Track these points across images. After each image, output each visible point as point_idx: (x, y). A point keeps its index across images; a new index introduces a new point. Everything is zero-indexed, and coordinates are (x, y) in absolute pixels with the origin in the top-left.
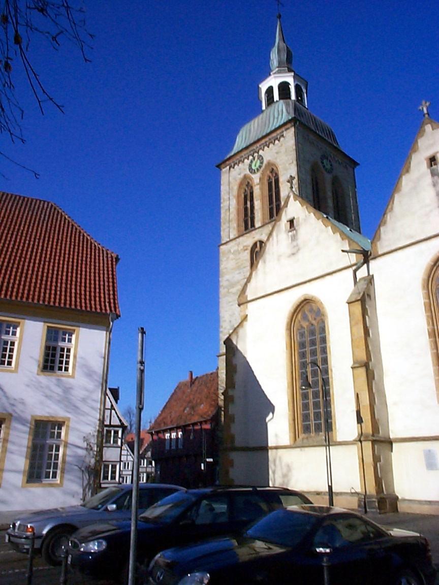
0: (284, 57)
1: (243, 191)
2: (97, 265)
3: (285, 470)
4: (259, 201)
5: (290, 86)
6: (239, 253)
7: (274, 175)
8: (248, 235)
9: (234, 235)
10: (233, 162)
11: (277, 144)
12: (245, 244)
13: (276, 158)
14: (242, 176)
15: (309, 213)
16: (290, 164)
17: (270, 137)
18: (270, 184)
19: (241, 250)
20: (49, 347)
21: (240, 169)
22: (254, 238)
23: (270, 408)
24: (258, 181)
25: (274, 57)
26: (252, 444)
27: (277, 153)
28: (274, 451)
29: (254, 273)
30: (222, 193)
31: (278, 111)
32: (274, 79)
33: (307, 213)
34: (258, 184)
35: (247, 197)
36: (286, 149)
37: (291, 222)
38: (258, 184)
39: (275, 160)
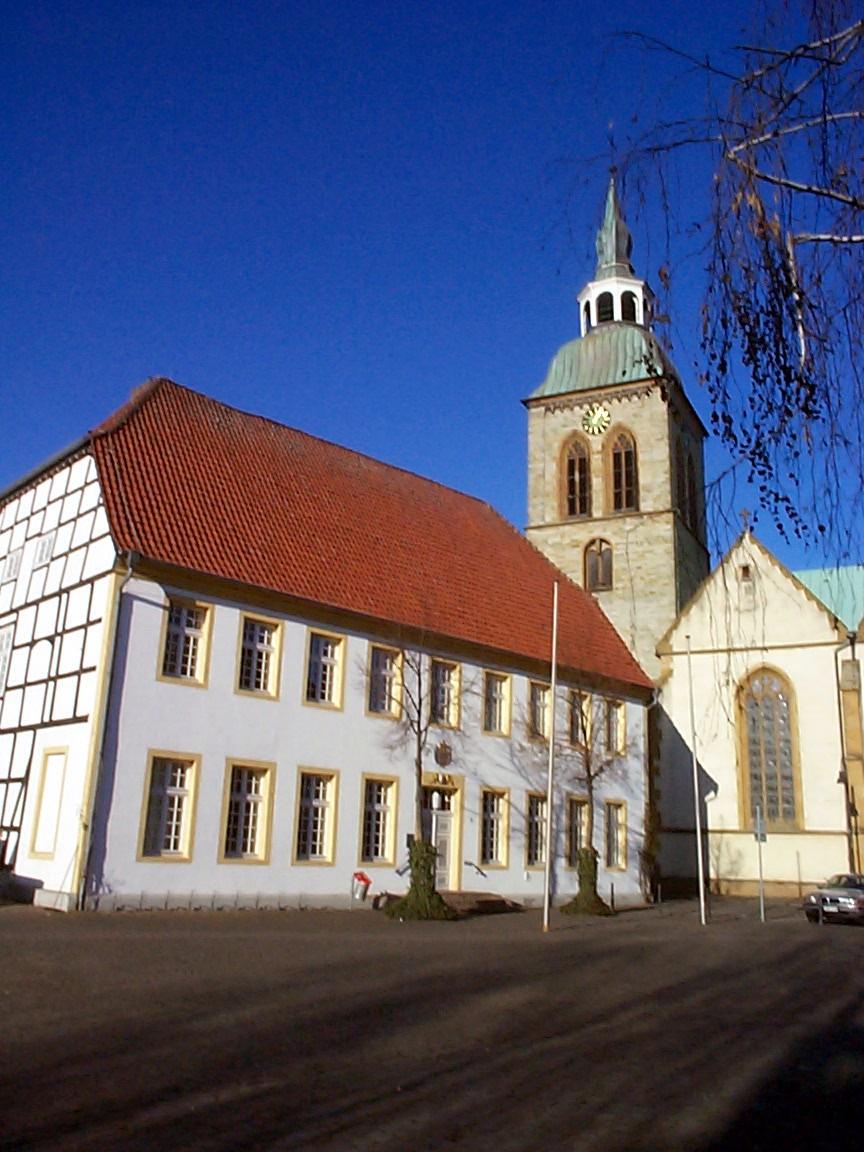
0: (624, 244)
1: (567, 452)
2: (131, 446)
3: (734, 857)
4: (600, 479)
5: (635, 299)
6: (563, 549)
7: (625, 445)
8: (581, 525)
9: (553, 519)
10: (554, 404)
11: (635, 403)
12: (575, 537)
13: (633, 423)
14: (569, 430)
15: (773, 564)
16: (658, 440)
17: (625, 387)
18: (617, 457)
19: (568, 544)
20: (196, 627)
21: (565, 418)
22: (591, 532)
23: (709, 785)
24: (600, 448)
25: (608, 240)
26: (680, 825)
27: (635, 415)
28: (718, 835)
29: (683, 620)
30: (532, 448)
31: (633, 348)
32: (615, 284)
33: (770, 564)
34: (598, 452)
35: (577, 468)
36: (652, 415)
37: (746, 569)
38: (598, 452)
39: (630, 426)
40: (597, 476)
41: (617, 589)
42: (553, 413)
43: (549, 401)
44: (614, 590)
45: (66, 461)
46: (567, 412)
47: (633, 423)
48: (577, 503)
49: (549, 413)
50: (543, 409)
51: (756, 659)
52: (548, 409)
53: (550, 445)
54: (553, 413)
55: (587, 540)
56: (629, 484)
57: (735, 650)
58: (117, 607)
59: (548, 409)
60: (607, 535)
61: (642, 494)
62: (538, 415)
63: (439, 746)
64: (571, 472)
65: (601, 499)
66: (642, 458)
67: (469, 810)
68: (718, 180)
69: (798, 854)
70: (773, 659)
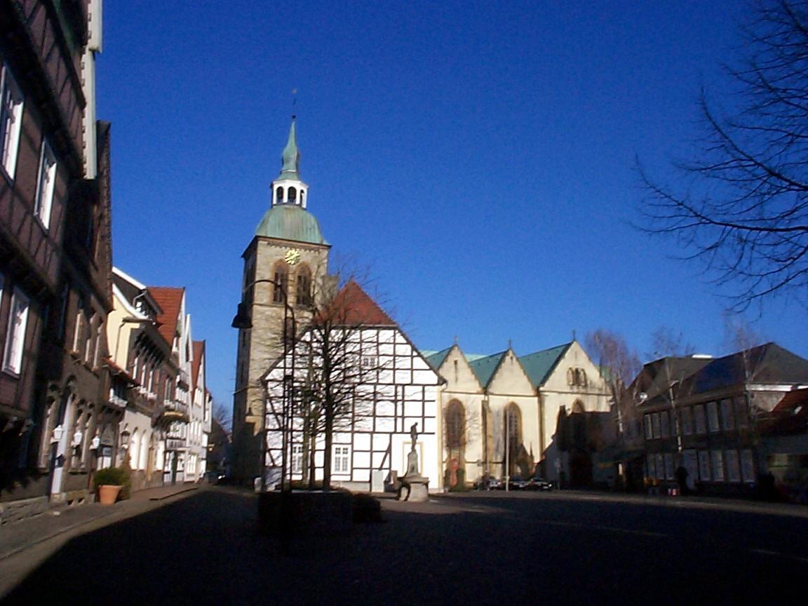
25: (291, 150)
43: (271, 240)
45: (50, 226)
46: (278, 248)
50: (266, 243)
51: (512, 399)
52: (269, 244)
53: (268, 262)
57: (374, 412)
59: (269, 244)
63: (18, 485)
67: (731, 230)
70: (516, 400)
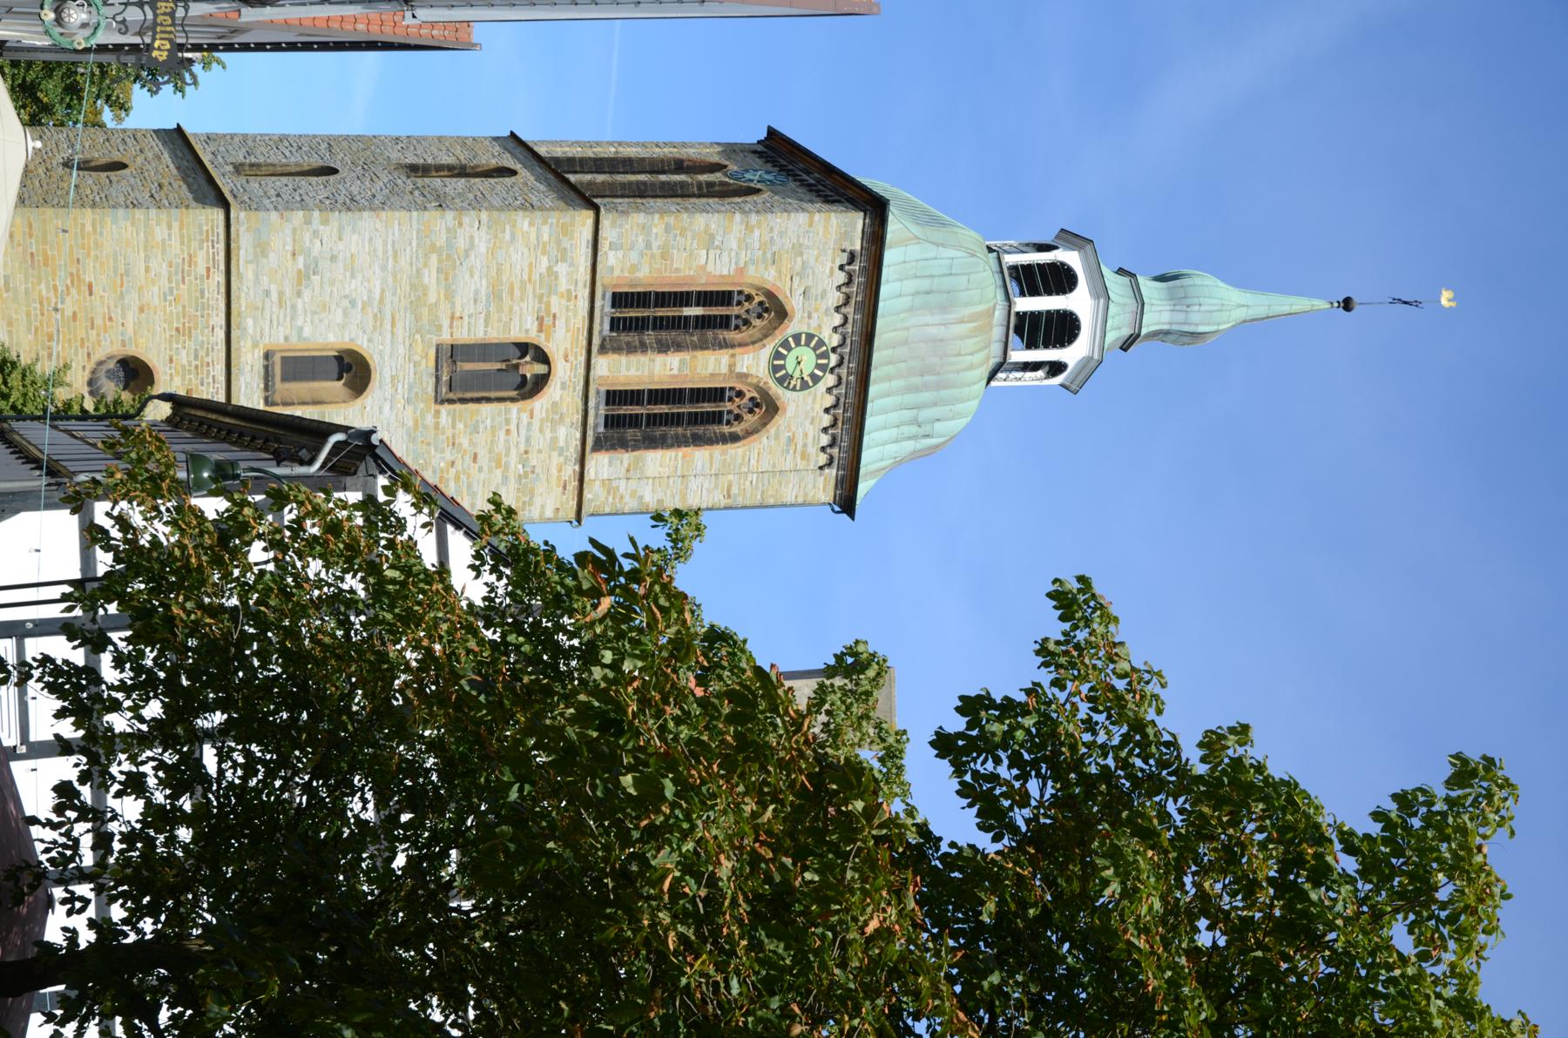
12: (560, 323)
27: (791, 440)
34: (732, 366)
35: (711, 313)
40: (682, 362)
41: (437, 412)
42: (841, 268)
44: (434, 407)
47: (777, 437)
48: (641, 315)
49: (844, 258)
52: (852, 257)
54: (841, 268)
55: (550, 348)
56: (654, 420)
58: (650, 336)
60: (552, 391)
61: (626, 457)
62: (845, 235)
64: (706, 298)
65: (633, 372)
66: (700, 456)
68: (267, 493)
69: (1417, 304)
